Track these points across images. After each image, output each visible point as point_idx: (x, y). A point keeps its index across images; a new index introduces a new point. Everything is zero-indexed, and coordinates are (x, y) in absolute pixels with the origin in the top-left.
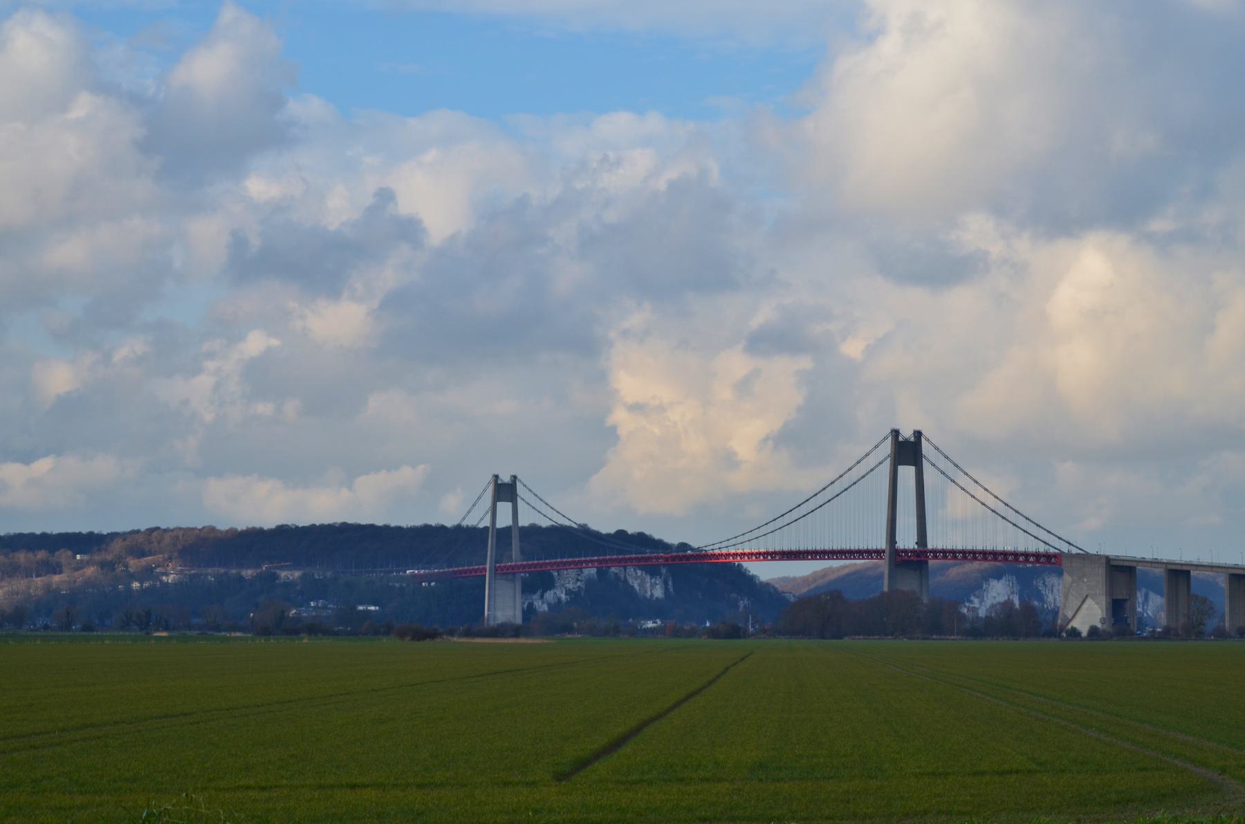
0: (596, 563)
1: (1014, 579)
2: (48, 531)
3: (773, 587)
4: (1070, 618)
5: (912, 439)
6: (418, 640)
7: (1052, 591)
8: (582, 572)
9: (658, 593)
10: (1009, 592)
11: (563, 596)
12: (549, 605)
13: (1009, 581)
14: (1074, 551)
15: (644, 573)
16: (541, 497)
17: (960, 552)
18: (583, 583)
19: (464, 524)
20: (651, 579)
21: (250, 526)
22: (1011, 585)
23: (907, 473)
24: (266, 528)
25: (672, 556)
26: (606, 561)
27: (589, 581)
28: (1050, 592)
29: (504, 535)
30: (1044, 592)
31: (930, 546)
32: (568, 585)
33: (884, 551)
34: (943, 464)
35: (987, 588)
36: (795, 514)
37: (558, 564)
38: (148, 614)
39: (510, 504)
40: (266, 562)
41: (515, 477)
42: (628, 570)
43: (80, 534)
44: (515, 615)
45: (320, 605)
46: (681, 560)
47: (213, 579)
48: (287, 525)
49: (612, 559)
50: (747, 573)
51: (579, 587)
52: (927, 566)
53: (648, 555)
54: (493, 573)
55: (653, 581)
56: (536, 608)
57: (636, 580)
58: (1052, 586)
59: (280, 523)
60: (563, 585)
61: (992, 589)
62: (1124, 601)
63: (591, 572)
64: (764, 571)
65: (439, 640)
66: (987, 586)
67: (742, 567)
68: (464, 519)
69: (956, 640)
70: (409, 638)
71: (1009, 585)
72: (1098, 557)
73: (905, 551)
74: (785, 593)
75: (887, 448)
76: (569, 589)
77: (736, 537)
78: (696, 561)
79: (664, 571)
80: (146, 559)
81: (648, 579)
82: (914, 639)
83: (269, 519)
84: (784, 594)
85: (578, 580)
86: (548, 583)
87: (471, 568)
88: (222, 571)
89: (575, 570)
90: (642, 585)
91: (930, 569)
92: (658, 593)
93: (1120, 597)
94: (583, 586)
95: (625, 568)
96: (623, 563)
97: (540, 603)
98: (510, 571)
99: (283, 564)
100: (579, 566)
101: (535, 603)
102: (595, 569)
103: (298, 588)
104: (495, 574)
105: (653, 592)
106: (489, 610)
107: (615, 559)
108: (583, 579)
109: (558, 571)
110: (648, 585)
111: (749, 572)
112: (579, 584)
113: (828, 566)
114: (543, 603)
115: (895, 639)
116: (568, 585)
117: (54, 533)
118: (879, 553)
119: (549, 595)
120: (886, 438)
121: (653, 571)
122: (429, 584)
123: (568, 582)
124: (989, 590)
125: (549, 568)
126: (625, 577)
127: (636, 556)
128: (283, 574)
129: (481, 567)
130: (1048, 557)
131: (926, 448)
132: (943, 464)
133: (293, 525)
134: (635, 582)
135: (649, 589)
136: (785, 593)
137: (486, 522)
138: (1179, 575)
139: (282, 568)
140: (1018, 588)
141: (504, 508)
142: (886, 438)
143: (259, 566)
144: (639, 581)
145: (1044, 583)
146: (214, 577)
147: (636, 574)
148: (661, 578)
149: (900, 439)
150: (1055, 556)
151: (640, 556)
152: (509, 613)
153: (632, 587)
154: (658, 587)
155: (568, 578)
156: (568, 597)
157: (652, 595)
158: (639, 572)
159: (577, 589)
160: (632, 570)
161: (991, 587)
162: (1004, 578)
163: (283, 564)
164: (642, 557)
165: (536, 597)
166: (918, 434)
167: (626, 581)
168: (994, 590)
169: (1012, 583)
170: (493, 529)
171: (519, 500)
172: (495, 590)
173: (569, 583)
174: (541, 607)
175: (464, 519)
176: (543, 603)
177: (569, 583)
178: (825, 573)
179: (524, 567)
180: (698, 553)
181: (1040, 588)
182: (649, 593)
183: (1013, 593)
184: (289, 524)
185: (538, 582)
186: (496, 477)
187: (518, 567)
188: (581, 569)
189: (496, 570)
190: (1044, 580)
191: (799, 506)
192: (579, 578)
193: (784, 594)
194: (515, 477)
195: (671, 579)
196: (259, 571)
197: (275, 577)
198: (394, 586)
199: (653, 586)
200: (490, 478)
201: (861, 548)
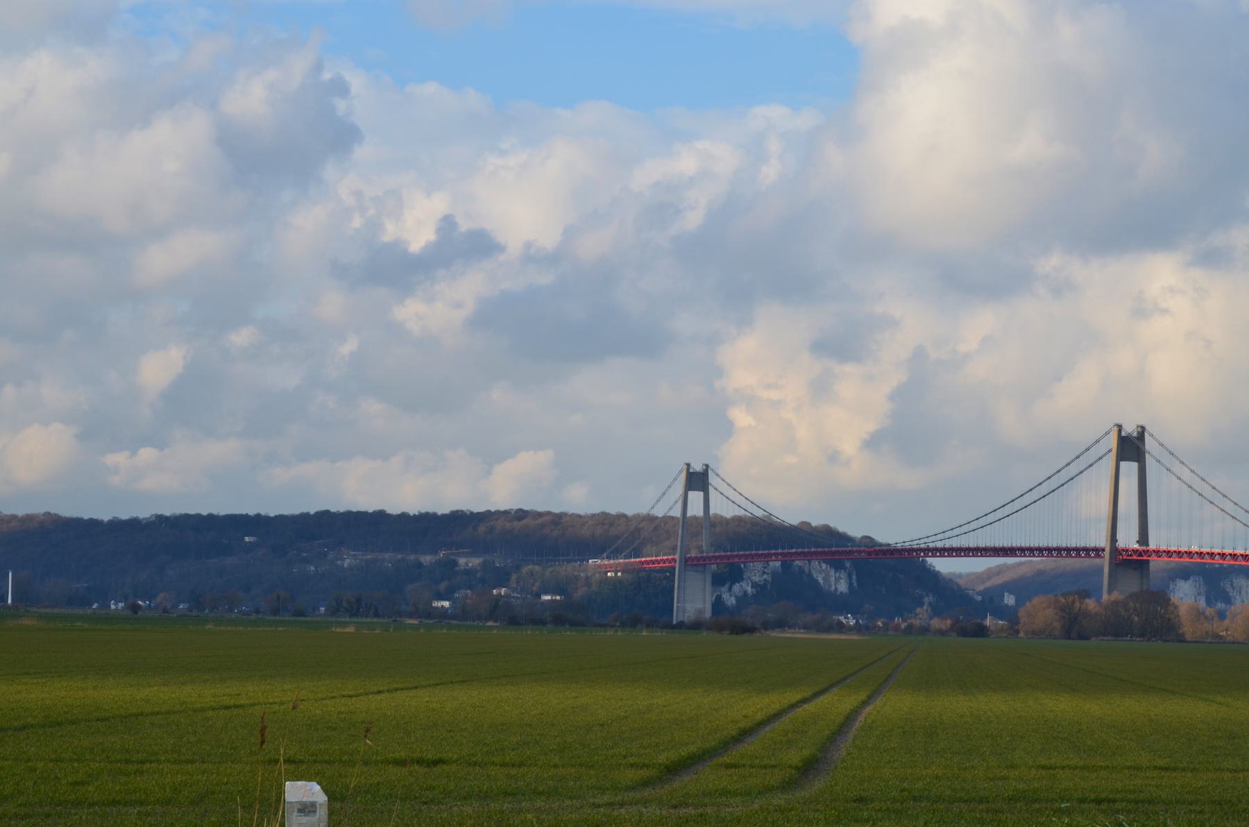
0: (780, 557)
1: (1201, 578)
2: (215, 512)
3: (957, 584)
6: (737, 634)
7: (1240, 593)
8: (768, 565)
9: (843, 587)
10: (1196, 594)
11: (749, 589)
12: (736, 597)
13: (1196, 581)
15: (829, 566)
16: (735, 487)
17: (1055, 549)
18: (770, 575)
20: (835, 573)
21: (423, 511)
22: (1197, 585)
23: (1129, 469)
24: (439, 513)
25: (875, 550)
26: (791, 554)
27: (774, 575)
28: (1238, 594)
30: (1231, 594)
31: (1152, 546)
33: (1103, 550)
34: (1166, 459)
35: (1174, 589)
36: (1008, 510)
37: (746, 556)
38: (359, 600)
39: (701, 494)
40: (444, 548)
42: (812, 563)
43: (247, 515)
44: (705, 607)
45: (503, 593)
47: (390, 565)
48: (461, 511)
49: (758, 554)
50: (932, 569)
51: (765, 580)
52: (1149, 566)
53: (850, 548)
54: (683, 564)
55: (837, 575)
56: (724, 602)
57: (820, 574)
58: (1240, 588)
59: (455, 508)
60: (749, 577)
61: (1178, 590)
63: (776, 564)
65: (758, 634)
66: (1174, 586)
67: (927, 562)
68: (653, 508)
69: (1109, 640)
70: (728, 632)
71: (1196, 586)
74: (969, 590)
75: (1112, 442)
76: (756, 582)
77: (944, 532)
78: (840, 557)
79: (848, 565)
80: (318, 542)
81: (832, 572)
82: (1168, 641)
83: (366, 502)
84: (967, 591)
85: (764, 573)
87: (659, 558)
88: (400, 556)
89: (762, 563)
90: (826, 579)
91: (1151, 568)
92: (843, 587)
94: (770, 579)
95: (809, 561)
96: (808, 556)
97: (728, 597)
98: (701, 562)
99: (461, 551)
100: (766, 558)
101: (723, 596)
102: (780, 562)
103: (479, 575)
104: (685, 565)
105: (838, 586)
106: (678, 602)
107: (801, 552)
108: (769, 571)
109: (744, 563)
110: (833, 579)
111: (934, 567)
112: (765, 576)
113: (1002, 563)
114: (731, 596)
115: (1149, 640)
116: (754, 578)
117: (221, 514)
118: (1098, 551)
120: (1107, 433)
121: (838, 566)
122: (616, 574)
123: (757, 573)
124: (1176, 590)
125: (736, 560)
126: (810, 570)
127: (837, 549)
128: (462, 561)
131: (1149, 444)
132: (1166, 459)
133: (468, 510)
134: (819, 575)
135: (833, 583)
136: (969, 590)
137: (677, 512)
139: (459, 555)
140: (1205, 590)
141: (696, 497)
143: (436, 553)
144: (823, 575)
145: (1232, 585)
146: (391, 563)
147: (821, 567)
148: (845, 572)
149: (1123, 434)
151: (840, 549)
152: (699, 605)
153: (816, 581)
155: (753, 570)
156: (754, 590)
157: (836, 589)
158: (824, 566)
159: (763, 582)
160: (817, 563)
161: (1178, 587)
162: (1192, 578)
163: (461, 551)
164: (843, 551)
165: (724, 589)
167: (810, 575)
168: (1181, 591)
169: (1199, 584)
170: (683, 522)
172: (685, 581)
173: (755, 576)
174: (730, 601)
175: (653, 508)
176: (731, 596)
177: (755, 576)
178: (1000, 570)
179: (715, 558)
180: (880, 548)
181: (1228, 590)
182: (833, 587)
184: (464, 509)
185: (729, 575)
187: (710, 558)
188: (767, 562)
190: (1232, 581)
191: (1013, 501)
192: (766, 571)
193: (967, 591)
195: (855, 573)
196: (437, 558)
197: (455, 563)
198: (580, 575)
199: (837, 580)
201: (1023, 545)
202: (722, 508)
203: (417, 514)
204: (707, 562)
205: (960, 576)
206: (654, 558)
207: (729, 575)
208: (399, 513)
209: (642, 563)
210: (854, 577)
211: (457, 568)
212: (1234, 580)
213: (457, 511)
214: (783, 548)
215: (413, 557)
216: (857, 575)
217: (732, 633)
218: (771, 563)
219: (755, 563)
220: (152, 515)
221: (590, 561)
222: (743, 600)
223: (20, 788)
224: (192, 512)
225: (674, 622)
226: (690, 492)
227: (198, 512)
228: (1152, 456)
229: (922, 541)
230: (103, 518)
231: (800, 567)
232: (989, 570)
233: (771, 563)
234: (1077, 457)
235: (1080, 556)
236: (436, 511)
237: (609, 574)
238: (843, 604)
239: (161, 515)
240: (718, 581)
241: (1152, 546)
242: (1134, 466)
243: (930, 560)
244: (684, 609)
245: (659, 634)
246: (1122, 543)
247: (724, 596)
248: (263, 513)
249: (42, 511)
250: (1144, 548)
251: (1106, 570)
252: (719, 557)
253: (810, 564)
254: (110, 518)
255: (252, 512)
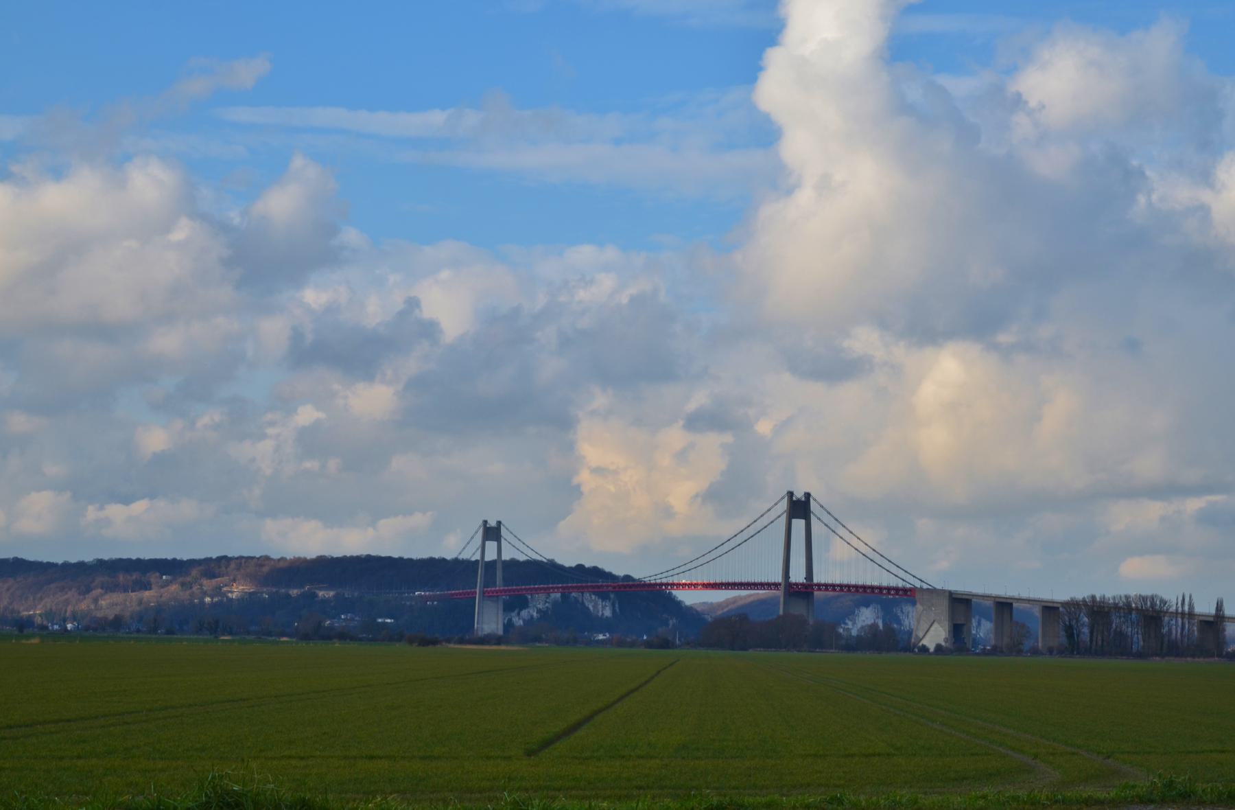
2: (142, 557)
4: (921, 637)
5: (803, 499)
6: (423, 646)
9: (608, 613)
11: (535, 614)
12: (524, 620)
14: (925, 586)
16: (739, 531)
19: (461, 557)
20: (602, 602)
23: (799, 525)
27: (555, 603)
29: (491, 566)
30: (901, 618)
32: (538, 606)
34: (826, 518)
41: (499, 523)
42: (585, 595)
44: (497, 628)
46: (460, 595)
51: (547, 607)
53: (600, 584)
58: (908, 613)
62: (963, 625)
64: (688, 598)
65: (439, 646)
67: (672, 594)
72: (943, 591)
73: (797, 584)
75: (784, 505)
81: (600, 602)
85: (546, 602)
86: (524, 604)
87: (465, 591)
90: (595, 606)
92: (608, 613)
93: (959, 622)
96: (581, 589)
97: (517, 619)
100: (547, 591)
103: (332, 604)
105: (604, 612)
106: (478, 623)
112: (547, 605)
114: (519, 619)
116: (538, 606)
117: (146, 558)
118: (776, 585)
119: (524, 613)
120: (783, 498)
121: (604, 596)
123: (539, 603)
128: (321, 593)
129: (473, 590)
130: (905, 590)
132: (826, 518)
135: (600, 610)
137: (477, 557)
138: (1004, 606)
139: (320, 589)
141: (491, 546)
142: (783, 498)
143: (303, 587)
144: (593, 604)
145: (902, 611)
147: (591, 598)
149: (794, 499)
150: (911, 590)
151: (593, 584)
153: (588, 608)
154: (607, 608)
157: (603, 614)
158: (593, 597)
162: (871, 606)
165: (514, 614)
166: (808, 495)
167: (583, 603)
171: (502, 540)
174: (518, 622)
178: (735, 600)
179: (505, 591)
182: (600, 613)
183: (878, 617)
185: (516, 603)
186: (485, 522)
188: (549, 594)
189: (484, 593)
190: (902, 608)
192: (548, 600)
194: (499, 523)
196: (302, 590)
197: (315, 596)
199: (603, 608)
200: (481, 522)
202: (506, 556)
203: (292, 558)
204: (499, 594)
205: (696, 604)
206: (461, 591)
207: (516, 603)
208: (314, 556)
209: (452, 595)
210: (617, 605)
211: (316, 599)
212: (904, 608)
213: (321, 556)
214: (517, 585)
215: (283, 591)
216: (619, 603)
217: (646, 648)
218: (551, 595)
219: (540, 595)
220: (94, 560)
221: (416, 593)
222: (529, 622)
223: (222, 784)
224: (125, 557)
225: (1134, 650)
226: (487, 543)
227: (129, 557)
228: (815, 516)
229: (652, 578)
230: (58, 562)
231: (575, 598)
232: (727, 600)
233: (551, 595)
234: (762, 516)
235: (873, 592)
236: (306, 556)
237: (428, 603)
238: (604, 625)
239: (101, 559)
240: (509, 608)
241: (815, 581)
242: (802, 522)
243: (674, 592)
244: (482, 629)
245: (892, 656)
246: (793, 579)
247: (514, 619)
248: (178, 558)
249: (11, 557)
250: (809, 583)
251: (782, 600)
252: (510, 591)
253: (583, 596)
254: (172, 558)
255: (170, 557)
